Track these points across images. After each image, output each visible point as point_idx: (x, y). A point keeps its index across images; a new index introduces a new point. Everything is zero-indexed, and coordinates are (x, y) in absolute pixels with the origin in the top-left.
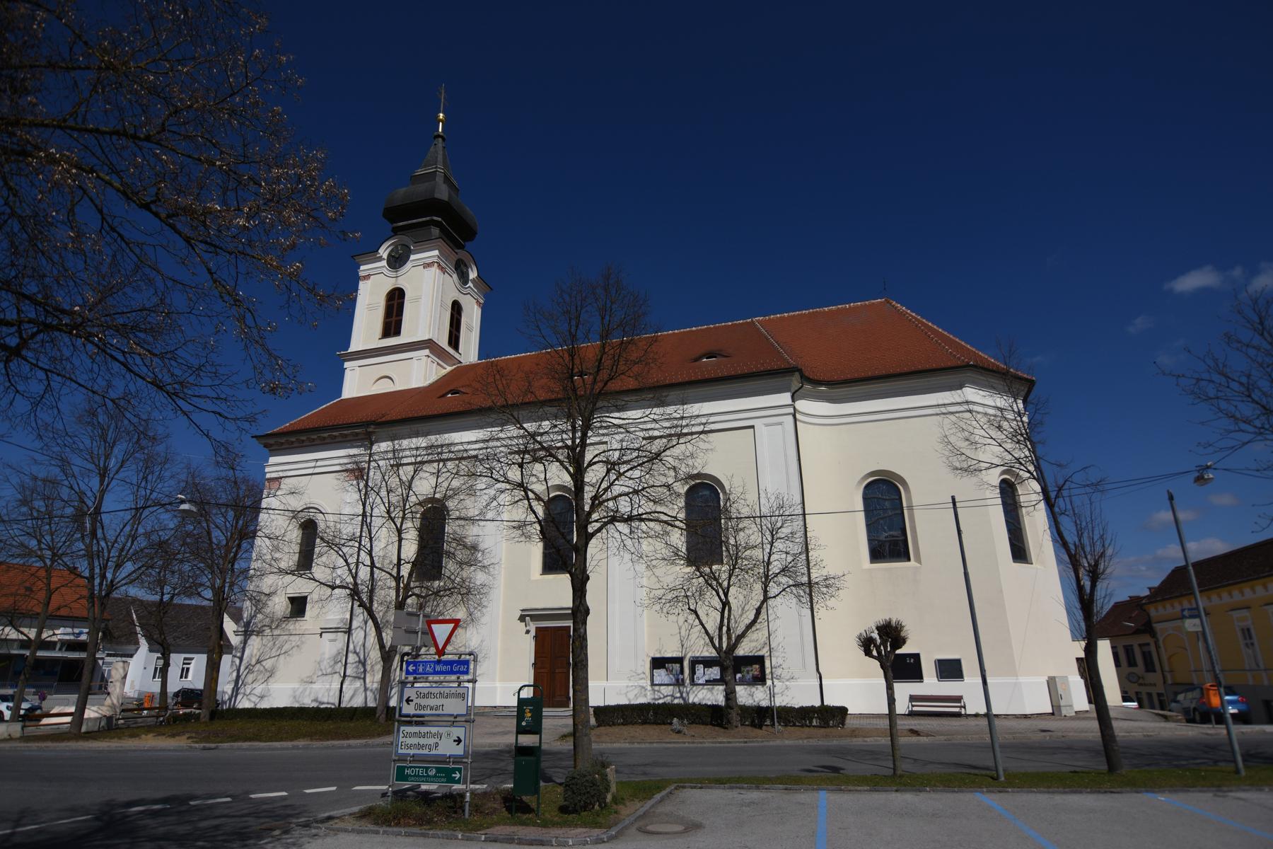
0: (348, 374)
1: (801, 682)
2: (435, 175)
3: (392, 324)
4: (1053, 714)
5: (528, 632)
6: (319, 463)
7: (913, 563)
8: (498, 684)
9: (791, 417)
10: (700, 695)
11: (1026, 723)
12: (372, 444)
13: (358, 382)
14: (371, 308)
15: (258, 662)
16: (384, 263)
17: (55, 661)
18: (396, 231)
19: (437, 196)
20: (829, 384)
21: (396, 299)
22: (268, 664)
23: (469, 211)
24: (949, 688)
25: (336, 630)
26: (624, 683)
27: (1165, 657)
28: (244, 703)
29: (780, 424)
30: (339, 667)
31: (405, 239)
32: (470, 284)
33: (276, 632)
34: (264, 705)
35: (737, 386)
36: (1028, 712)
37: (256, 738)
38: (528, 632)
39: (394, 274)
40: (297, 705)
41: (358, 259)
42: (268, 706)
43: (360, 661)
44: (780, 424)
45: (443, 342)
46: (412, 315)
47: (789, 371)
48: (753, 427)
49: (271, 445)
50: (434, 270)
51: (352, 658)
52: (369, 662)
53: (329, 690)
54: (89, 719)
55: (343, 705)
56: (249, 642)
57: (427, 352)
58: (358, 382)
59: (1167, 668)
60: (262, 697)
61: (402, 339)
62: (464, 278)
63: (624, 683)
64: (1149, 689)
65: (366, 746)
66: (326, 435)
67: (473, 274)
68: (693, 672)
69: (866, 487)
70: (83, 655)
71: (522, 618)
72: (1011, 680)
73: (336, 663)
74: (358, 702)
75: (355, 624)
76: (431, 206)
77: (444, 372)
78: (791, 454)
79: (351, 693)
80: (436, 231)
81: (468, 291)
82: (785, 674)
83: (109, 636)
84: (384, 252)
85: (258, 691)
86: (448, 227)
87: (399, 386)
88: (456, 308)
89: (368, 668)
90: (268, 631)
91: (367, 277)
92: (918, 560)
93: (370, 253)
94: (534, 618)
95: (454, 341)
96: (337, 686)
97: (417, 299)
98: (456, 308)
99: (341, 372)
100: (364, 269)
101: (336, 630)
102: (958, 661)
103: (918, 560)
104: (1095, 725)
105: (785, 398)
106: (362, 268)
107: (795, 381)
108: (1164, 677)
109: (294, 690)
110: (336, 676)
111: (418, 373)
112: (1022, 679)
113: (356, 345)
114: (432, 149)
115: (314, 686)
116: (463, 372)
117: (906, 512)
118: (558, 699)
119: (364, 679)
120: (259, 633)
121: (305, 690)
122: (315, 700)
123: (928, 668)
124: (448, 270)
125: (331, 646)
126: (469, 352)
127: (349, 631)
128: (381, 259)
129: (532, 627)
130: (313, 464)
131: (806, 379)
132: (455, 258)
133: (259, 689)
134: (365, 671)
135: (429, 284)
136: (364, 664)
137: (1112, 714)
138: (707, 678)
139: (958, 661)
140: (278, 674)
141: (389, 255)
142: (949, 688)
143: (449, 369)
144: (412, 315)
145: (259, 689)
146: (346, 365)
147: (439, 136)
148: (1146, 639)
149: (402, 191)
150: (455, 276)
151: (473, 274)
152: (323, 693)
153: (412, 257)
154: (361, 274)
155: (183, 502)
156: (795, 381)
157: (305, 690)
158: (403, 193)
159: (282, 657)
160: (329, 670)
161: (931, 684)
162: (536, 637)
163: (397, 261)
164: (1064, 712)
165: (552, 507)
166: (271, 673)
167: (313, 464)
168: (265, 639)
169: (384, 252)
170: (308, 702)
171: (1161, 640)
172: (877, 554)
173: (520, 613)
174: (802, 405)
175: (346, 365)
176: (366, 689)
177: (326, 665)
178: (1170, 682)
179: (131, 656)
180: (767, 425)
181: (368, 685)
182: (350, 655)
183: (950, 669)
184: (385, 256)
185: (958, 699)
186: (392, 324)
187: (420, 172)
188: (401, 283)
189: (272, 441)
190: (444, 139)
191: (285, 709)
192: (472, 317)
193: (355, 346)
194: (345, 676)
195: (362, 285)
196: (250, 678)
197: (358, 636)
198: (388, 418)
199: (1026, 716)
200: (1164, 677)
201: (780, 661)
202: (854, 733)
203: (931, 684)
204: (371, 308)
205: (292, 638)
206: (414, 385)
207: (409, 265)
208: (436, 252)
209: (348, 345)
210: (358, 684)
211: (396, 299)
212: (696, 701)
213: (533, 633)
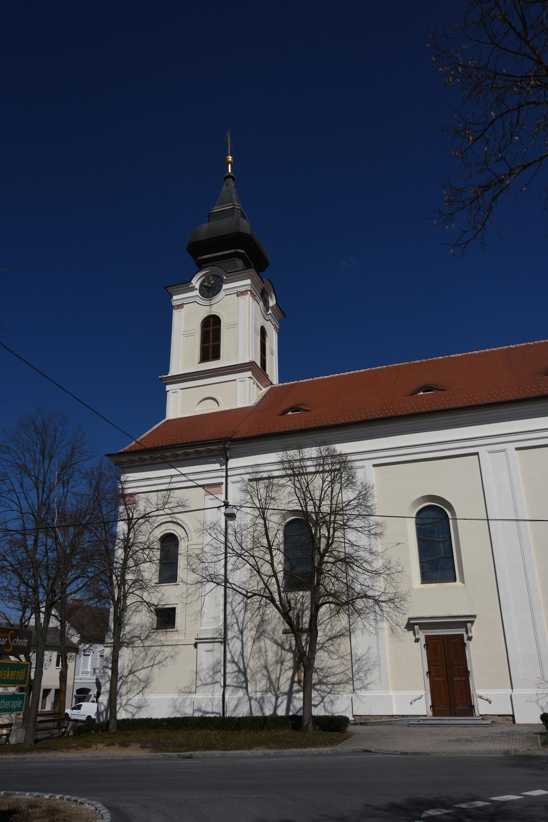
2: (229, 210)
5: (417, 640)
6: (174, 479)
7: (458, 583)
8: (392, 693)
12: (227, 460)
13: (181, 404)
14: (187, 334)
15: (131, 672)
16: (197, 293)
18: (200, 266)
21: (211, 328)
22: (142, 674)
25: (213, 640)
26: (533, 691)
29: (504, 451)
30: (219, 677)
31: (216, 270)
33: (147, 643)
34: (143, 715)
35: (482, 414)
38: (417, 640)
39: (208, 303)
40: (178, 715)
41: (170, 290)
42: (144, 717)
43: (239, 671)
44: (504, 451)
46: (224, 340)
48: (477, 454)
49: (123, 463)
50: (248, 297)
51: (231, 668)
52: (249, 671)
53: (212, 700)
55: (228, 715)
57: (249, 374)
58: (181, 404)
60: (139, 708)
66: (181, 452)
67: (272, 302)
73: (216, 673)
74: (243, 712)
75: (230, 634)
79: (234, 702)
80: (240, 263)
84: (196, 282)
87: (224, 407)
88: (263, 333)
89: (249, 677)
90: (138, 643)
91: (181, 306)
92: (463, 581)
93: (184, 284)
94: (424, 626)
96: (218, 695)
97: (234, 325)
98: (263, 333)
99: (164, 394)
100: (177, 299)
101: (213, 640)
103: (463, 581)
106: (175, 298)
109: (174, 701)
110: (217, 686)
114: (225, 188)
115: (194, 696)
118: (460, 707)
119: (246, 688)
120: (130, 644)
121: (184, 701)
122: (199, 710)
125: (208, 656)
127: (224, 641)
128: (193, 289)
129: (422, 635)
130: (168, 480)
133: (136, 699)
134: (246, 681)
136: (245, 674)
140: (153, 685)
141: (202, 285)
144: (224, 340)
145: (136, 699)
146: (168, 387)
151: (272, 302)
152: (206, 701)
153: (225, 287)
154: (174, 303)
157: (184, 701)
158: (205, 230)
159: (156, 668)
160: (209, 680)
162: (427, 645)
163: (210, 291)
166: (146, 683)
167: (168, 480)
168: (136, 651)
169: (196, 282)
170: (188, 712)
172: (427, 577)
175: (168, 387)
176: (250, 699)
177: (204, 675)
180: (490, 452)
182: (229, 665)
184: (197, 286)
187: (217, 209)
188: (216, 310)
189: (124, 459)
190: (234, 179)
191: (163, 720)
193: (174, 371)
194: (225, 686)
195: (177, 315)
197: (235, 646)
198: (238, 436)
204: (187, 334)
205: (164, 648)
206: (240, 404)
207: (222, 294)
208: (248, 281)
209: (167, 370)
210: (241, 693)
211: (211, 328)
213: (423, 641)
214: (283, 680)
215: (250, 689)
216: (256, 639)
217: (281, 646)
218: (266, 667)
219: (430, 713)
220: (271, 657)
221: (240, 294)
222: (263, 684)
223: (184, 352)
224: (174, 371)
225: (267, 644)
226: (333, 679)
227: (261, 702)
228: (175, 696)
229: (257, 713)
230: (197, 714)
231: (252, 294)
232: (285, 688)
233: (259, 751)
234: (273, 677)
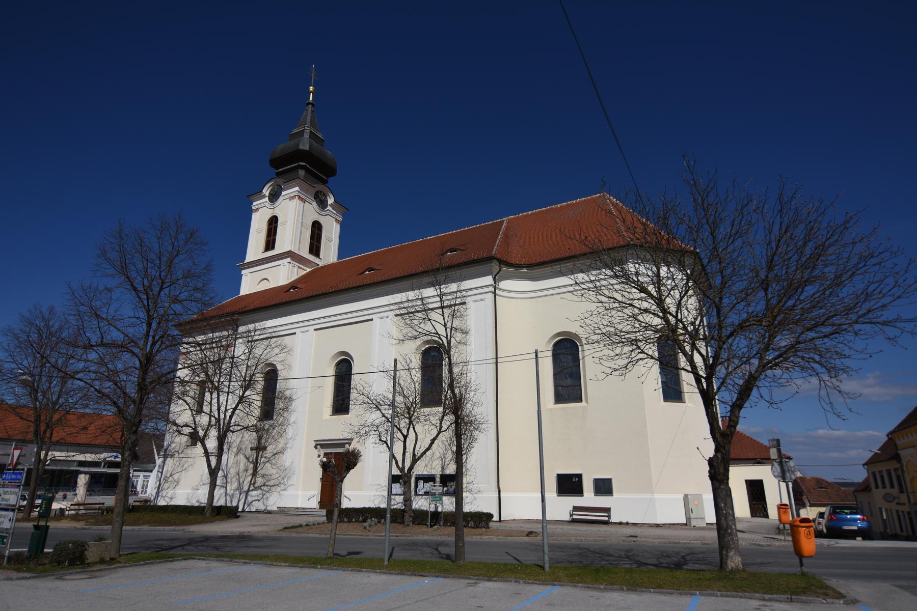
0: (244, 279)
1: (484, 495)
3: (270, 244)
4: (686, 524)
7: (584, 403)
8: (300, 492)
9: (491, 296)
10: (420, 503)
11: (658, 532)
15: (171, 475)
16: (267, 199)
17: (102, 474)
18: (279, 175)
19: (301, 147)
20: (529, 266)
21: (273, 223)
22: (176, 477)
23: (329, 153)
24: (602, 501)
27: (908, 479)
28: (162, 502)
29: (483, 300)
32: (329, 208)
34: (173, 503)
36: (659, 522)
37: (169, 524)
39: (272, 207)
45: (305, 252)
47: (490, 259)
52: (229, 476)
54: (56, 510)
56: (167, 462)
57: (289, 260)
59: (910, 490)
60: (171, 499)
61: (277, 251)
62: (322, 204)
63: (374, 493)
64: (900, 508)
65: (174, 530)
67: (331, 200)
68: (416, 486)
69: (556, 345)
70: (118, 471)
71: (316, 447)
72: (649, 496)
76: (297, 155)
77: (305, 272)
78: (508, 322)
80: (302, 173)
81: (327, 213)
82: (475, 489)
83: (135, 457)
84: (266, 191)
85: (169, 495)
86: (314, 171)
88: (317, 228)
89: (229, 480)
91: (257, 210)
92: (587, 402)
93: (258, 193)
94: (323, 446)
95: (315, 249)
97: (285, 223)
98: (317, 228)
102: (610, 480)
103: (587, 402)
104: (714, 534)
105: (489, 280)
106: (254, 204)
107: (495, 266)
108: (909, 498)
111: (283, 274)
112: (656, 496)
113: (249, 258)
116: (319, 272)
117: (581, 362)
120: (172, 456)
122: (198, 501)
123: (588, 486)
124: (308, 200)
126: (330, 253)
128: (264, 196)
129: (322, 452)
131: (503, 263)
132: (314, 191)
135: (291, 213)
137: (739, 526)
138: (424, 490)
139: (610, 480)
140: (181, 484)
142: (602, 501)
143: (309, 270)
145: (170, 493)
146: (243, 272)
147: (309, 103)
148: (893, 465)
149: (280, 147)
150: (314, 204)
151: (331, 200)
153: (283, 193)
154: (254, 208)
155: (22, 374)
156: (495, 266)
158: (282, 147)
161: (589, 498)
164: (693, 523)
165: (340, 366)
166: (177, 482)
169: (266, 191)
171: (904, 464)
173: (314, 444)
174: (505, 284)
178: (912, 502)
179: (151, 471)
180: (475, 301)
181: (228, 492)
183: (604, 487)
184: (267, 194)
185: (607, 510)
186: (270, 244)
192: (332, 231)
196: (166, 485)
198: (249, 308)
199: (658, 526)
200: (909, 498)
201: (472, 479)
202: (497, 532)
203: (589, 498)
207: (281, 198)
208: (297, 188)
210: (223, 491)
211: (273, 223)
212: (417, 507)
214: (245, 483)
215: (228, 488)
216: (236, 454)
217: (248, 459)
218: (238, 474)
219: (318, 507)
220: (242, 467)
221: (292, 198)
222: (235, 485)
223: (255, 248)
224: (248, 260)
225: (241, 457)
226: (271, 483)
227: (232, 496)
228: (190, 491)
229: (229, 505)
230: (197, 504)
231: (299, 197)
232: (246, 488)
233: (145, 528)
234: (241, 480)
